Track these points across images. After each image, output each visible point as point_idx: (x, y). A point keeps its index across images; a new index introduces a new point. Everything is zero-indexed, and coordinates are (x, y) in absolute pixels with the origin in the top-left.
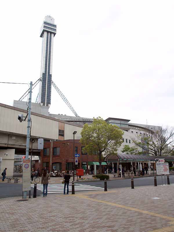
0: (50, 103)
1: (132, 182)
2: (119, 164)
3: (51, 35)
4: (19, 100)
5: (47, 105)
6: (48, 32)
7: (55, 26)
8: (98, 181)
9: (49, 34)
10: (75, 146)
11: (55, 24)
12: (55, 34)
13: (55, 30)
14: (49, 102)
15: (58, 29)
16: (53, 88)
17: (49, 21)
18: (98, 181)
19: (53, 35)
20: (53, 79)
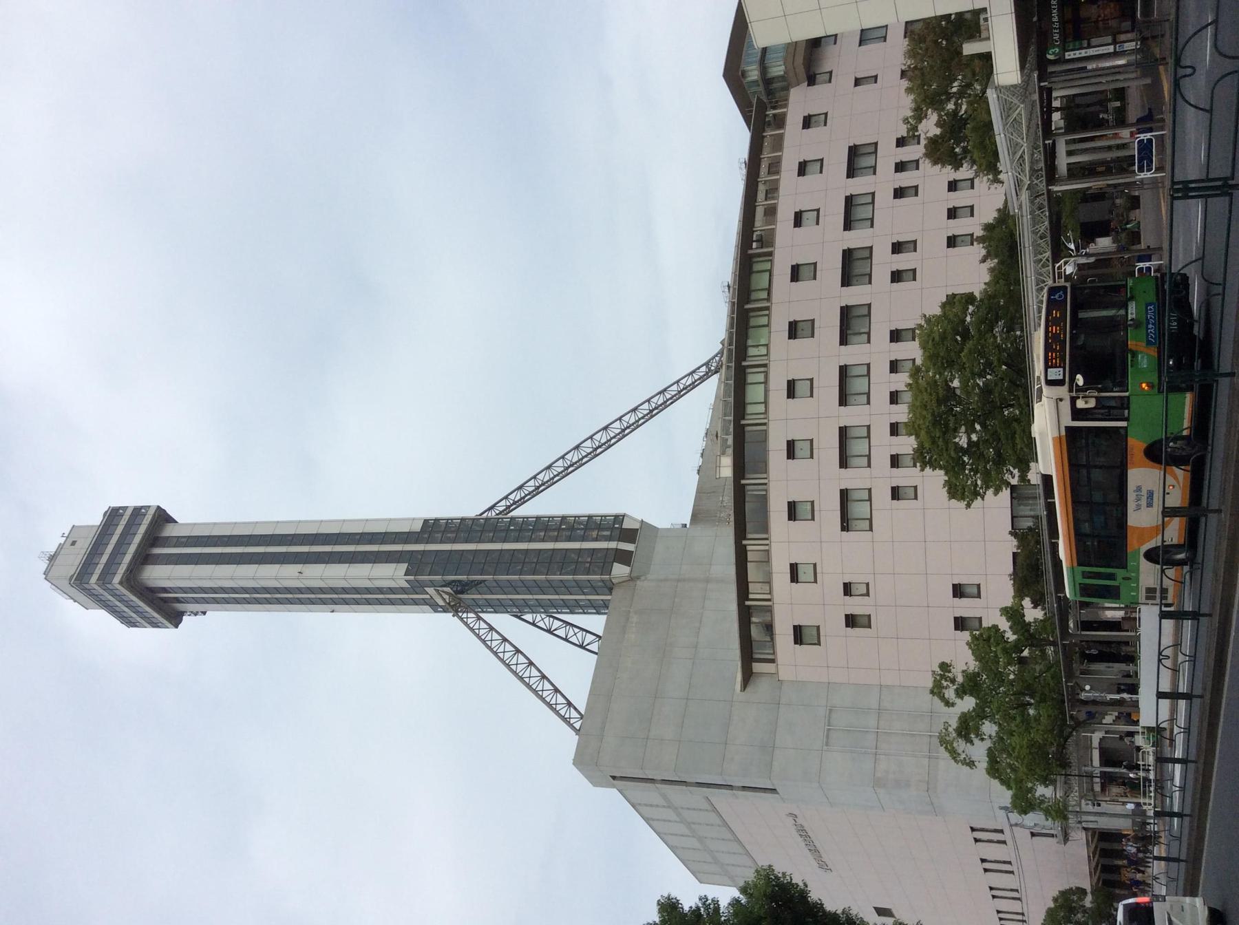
0: (619, 518)
1: (1177, 860)
2: (1193, 387)
3: (167, 542)
4: (577, 731)
5: (630, 535)
6: (144, 558)
7: (113, 515)
8: (1206, 520)
9: (157, 551)
10: (939, 173)
11: (96, 519)
12: (162, 517)
13: (138, 512)
14: (616, 527)
15: (129, 499)
16: (530, 510)
17: (72, 562)
18: (1206, 520)
19: (169, 531)
20: (469, 506)
